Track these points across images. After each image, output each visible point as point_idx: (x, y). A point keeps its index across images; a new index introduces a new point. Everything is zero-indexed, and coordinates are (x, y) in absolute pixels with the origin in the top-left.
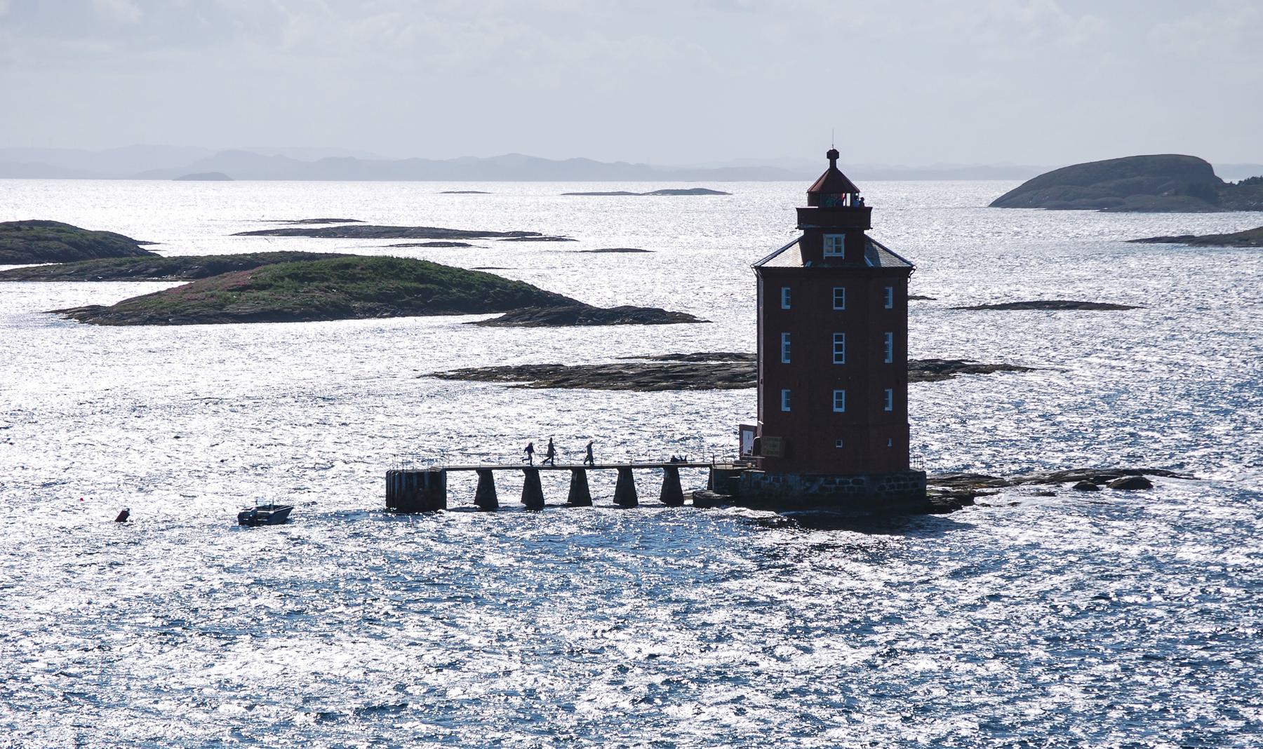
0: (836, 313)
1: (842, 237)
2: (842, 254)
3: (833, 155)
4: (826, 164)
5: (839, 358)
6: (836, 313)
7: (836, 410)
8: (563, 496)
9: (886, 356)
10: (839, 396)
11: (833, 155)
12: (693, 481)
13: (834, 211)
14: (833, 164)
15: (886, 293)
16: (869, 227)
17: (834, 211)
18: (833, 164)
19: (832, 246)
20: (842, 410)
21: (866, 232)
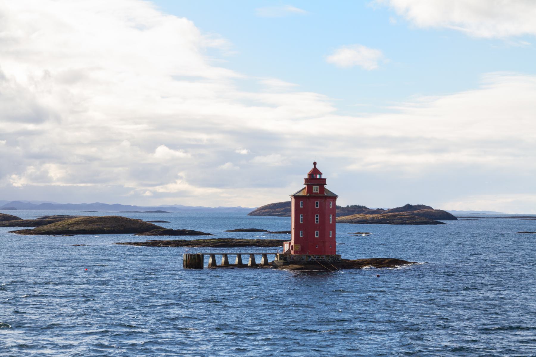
1: (318, 187)
2: (318, 192)
3: (315, 164)
4: (313, 167)
10: (317, 203)
11: (315, 164)
14: (315, 166)
18: (315, 166)
20: (318, 237)
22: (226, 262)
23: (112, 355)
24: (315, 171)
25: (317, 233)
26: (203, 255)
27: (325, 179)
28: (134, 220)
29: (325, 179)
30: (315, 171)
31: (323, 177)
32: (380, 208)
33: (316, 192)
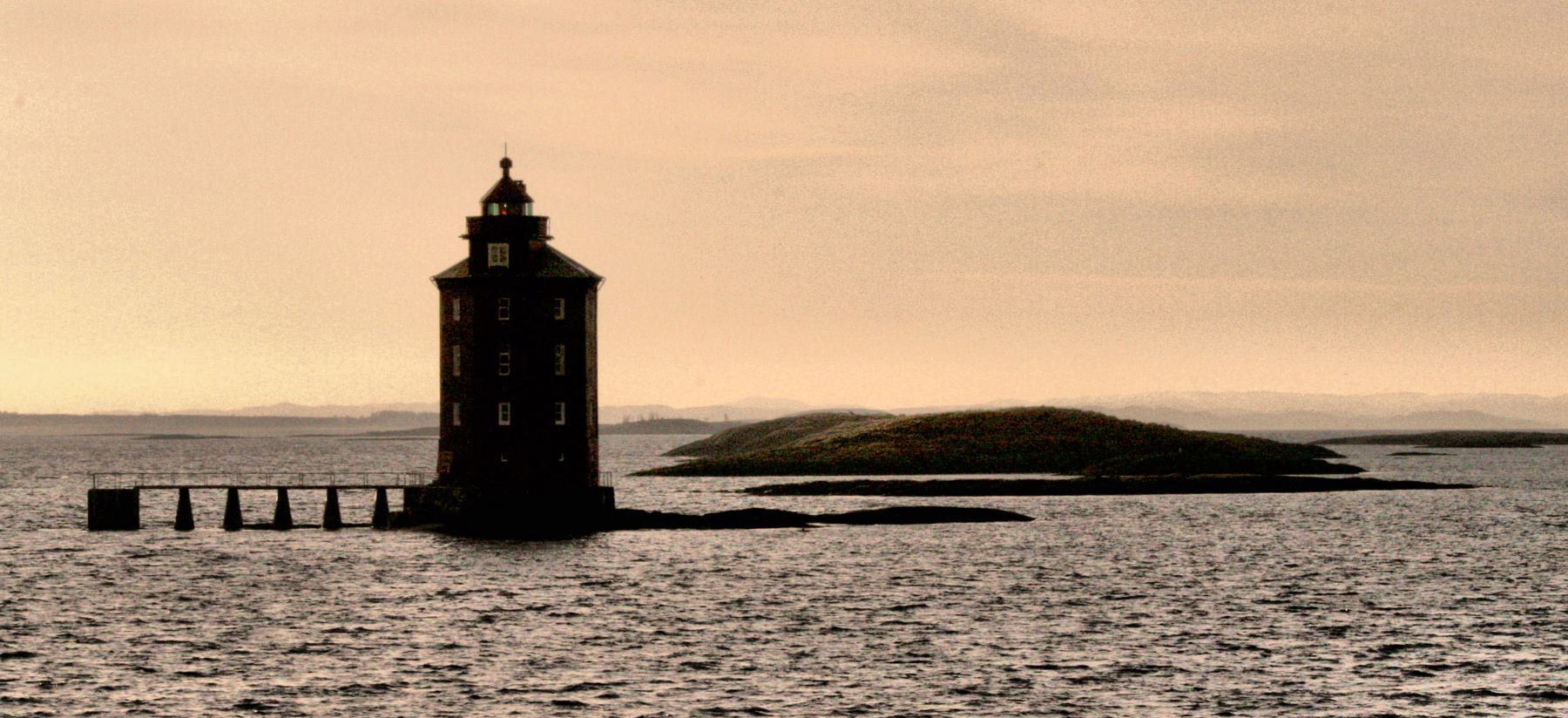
0: (517, 309)
1: (506, 246)
2: (506, 263)
3: (506, 164)
4: (498, 175)
5: (504, 369)
6: (517, 309)
7: (501, 423)
8: (269, 514)
9: (558, 312)
11: (506, 164)
12: (357, 506)
13: (507, 221)
14: (506, 174)
15: (559, 408)
16: (550, 238)
17: (507, 221)
18: (506, 174)
19: (498, 254)
20: (508, 423)
21: (549, 243)
22: (283, 508)
23: (173, 711)
24: (509, 193)
25: (505, 408)
26: (137, 489)
27: (545, 219)
28: (1253, 439)
29: (545, 219)
30: (509, 193)
31: (537, 210)
32: (529, 191)
33: (499, 263)
